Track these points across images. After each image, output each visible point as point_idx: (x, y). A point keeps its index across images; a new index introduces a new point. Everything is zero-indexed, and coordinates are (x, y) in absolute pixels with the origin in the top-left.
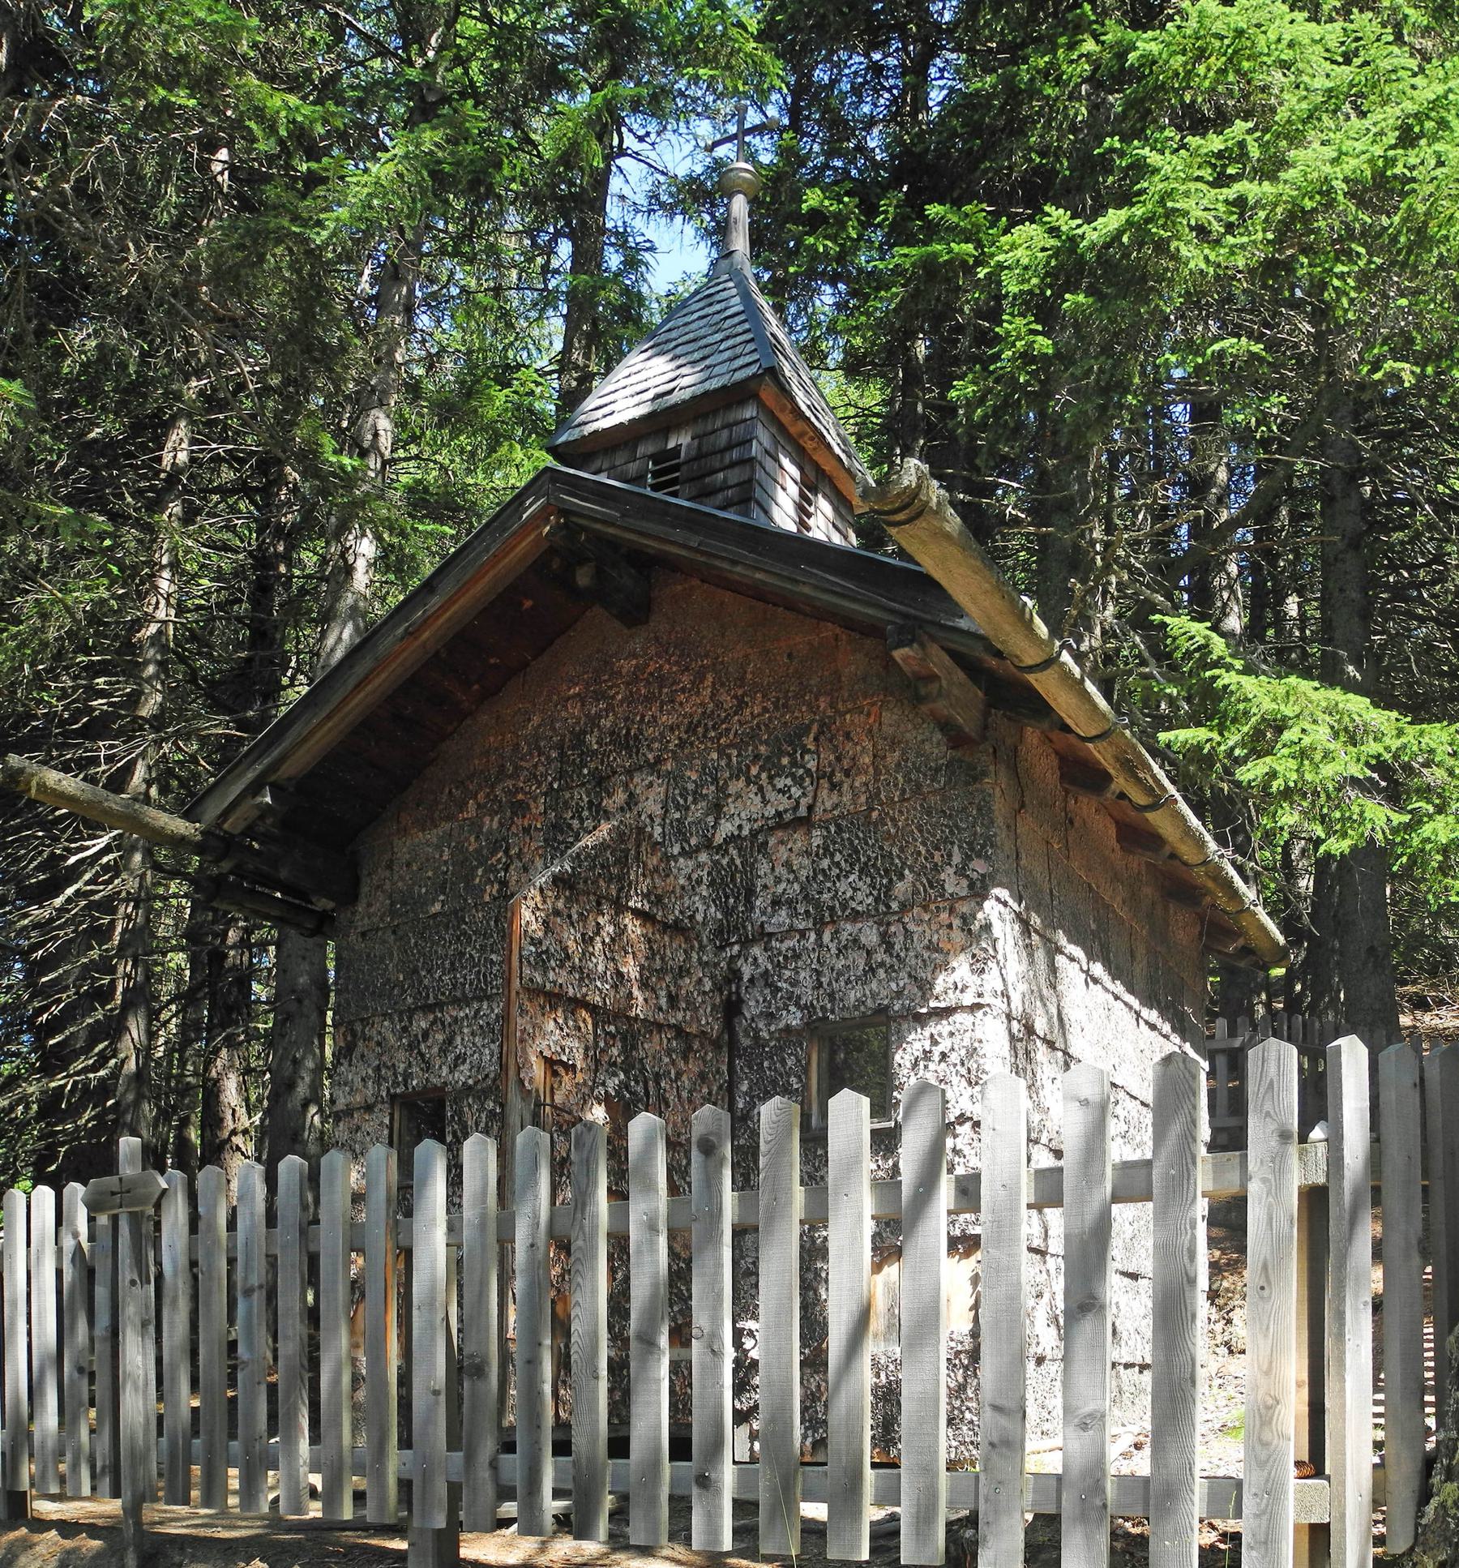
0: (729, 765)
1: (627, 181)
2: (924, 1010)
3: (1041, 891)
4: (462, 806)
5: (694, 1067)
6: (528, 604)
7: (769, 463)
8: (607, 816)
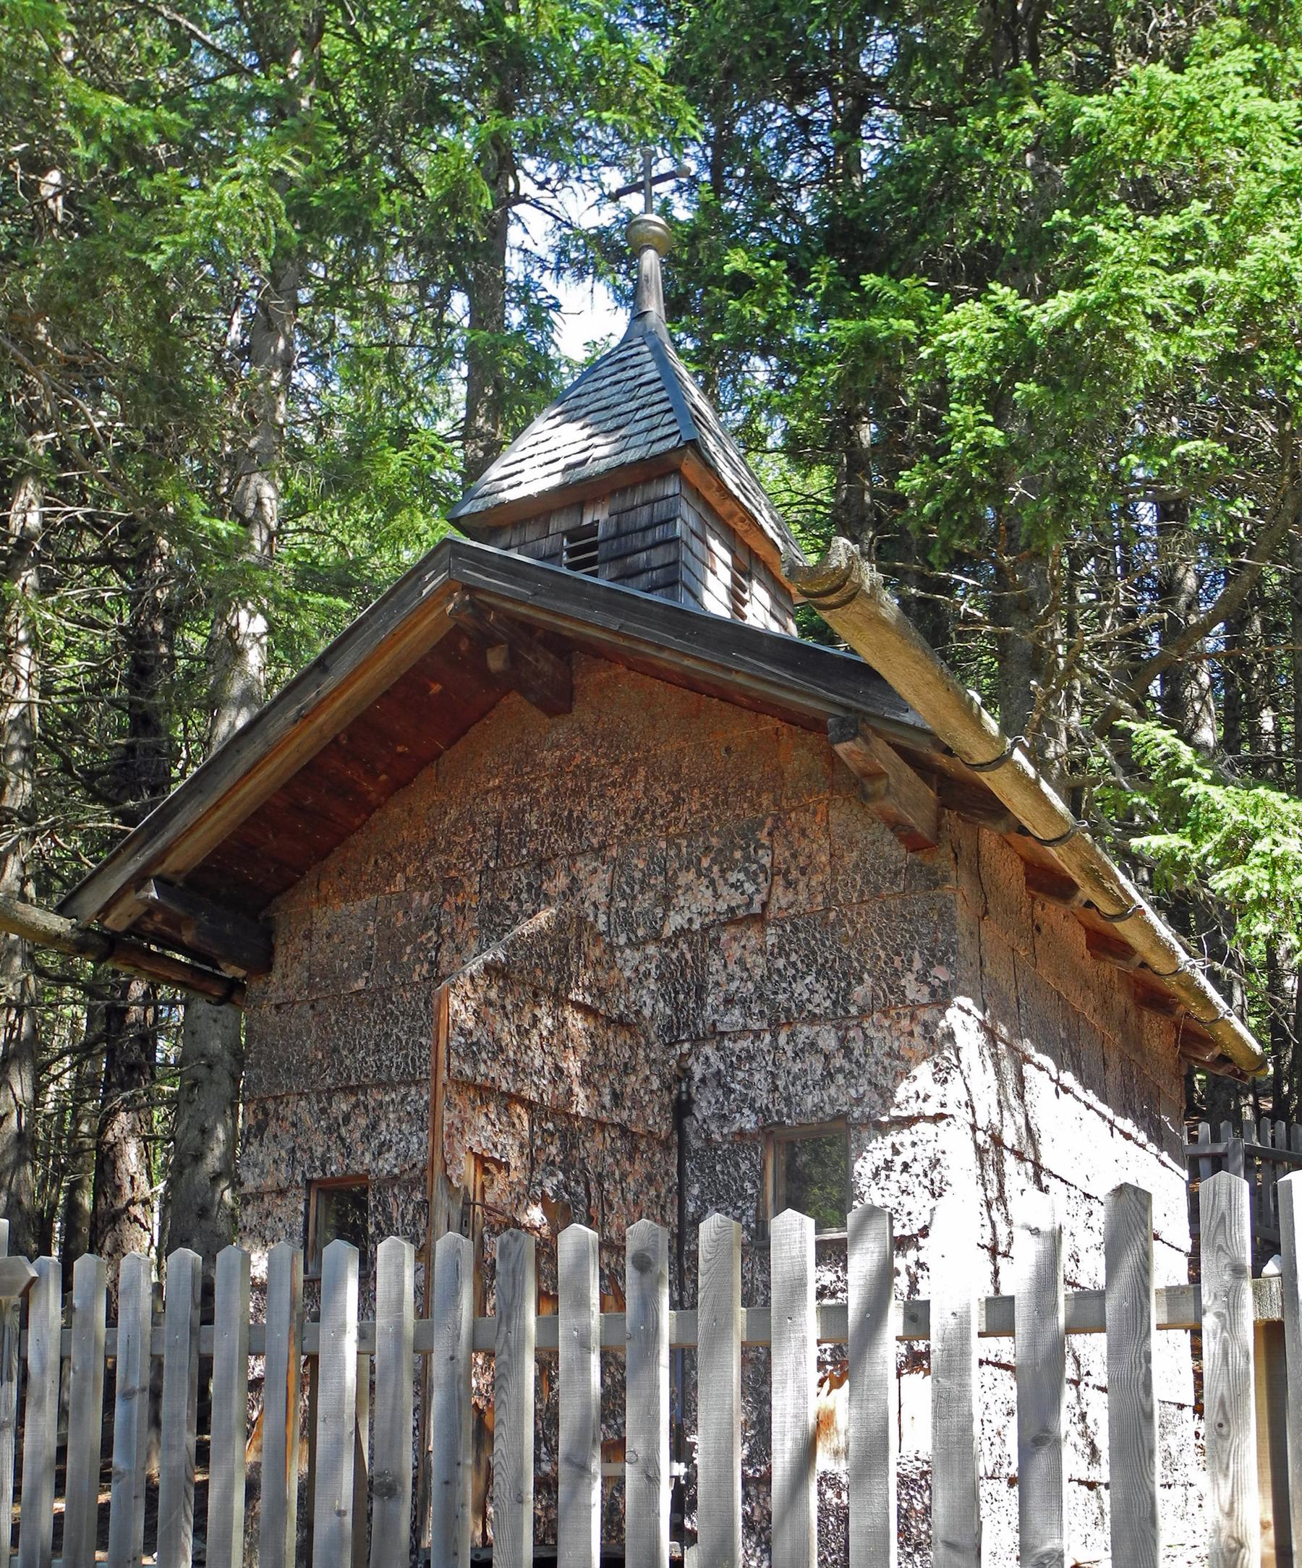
0: (678, 855)
1: (526, 231)
2: (885, 1119)
3: (1007, 999)
4: (389, 879)
5: (640, 1168)
6: (436, 688)
7: (695, 544)
8: (548, 900)
